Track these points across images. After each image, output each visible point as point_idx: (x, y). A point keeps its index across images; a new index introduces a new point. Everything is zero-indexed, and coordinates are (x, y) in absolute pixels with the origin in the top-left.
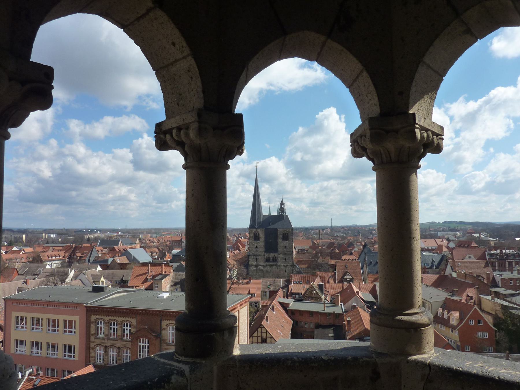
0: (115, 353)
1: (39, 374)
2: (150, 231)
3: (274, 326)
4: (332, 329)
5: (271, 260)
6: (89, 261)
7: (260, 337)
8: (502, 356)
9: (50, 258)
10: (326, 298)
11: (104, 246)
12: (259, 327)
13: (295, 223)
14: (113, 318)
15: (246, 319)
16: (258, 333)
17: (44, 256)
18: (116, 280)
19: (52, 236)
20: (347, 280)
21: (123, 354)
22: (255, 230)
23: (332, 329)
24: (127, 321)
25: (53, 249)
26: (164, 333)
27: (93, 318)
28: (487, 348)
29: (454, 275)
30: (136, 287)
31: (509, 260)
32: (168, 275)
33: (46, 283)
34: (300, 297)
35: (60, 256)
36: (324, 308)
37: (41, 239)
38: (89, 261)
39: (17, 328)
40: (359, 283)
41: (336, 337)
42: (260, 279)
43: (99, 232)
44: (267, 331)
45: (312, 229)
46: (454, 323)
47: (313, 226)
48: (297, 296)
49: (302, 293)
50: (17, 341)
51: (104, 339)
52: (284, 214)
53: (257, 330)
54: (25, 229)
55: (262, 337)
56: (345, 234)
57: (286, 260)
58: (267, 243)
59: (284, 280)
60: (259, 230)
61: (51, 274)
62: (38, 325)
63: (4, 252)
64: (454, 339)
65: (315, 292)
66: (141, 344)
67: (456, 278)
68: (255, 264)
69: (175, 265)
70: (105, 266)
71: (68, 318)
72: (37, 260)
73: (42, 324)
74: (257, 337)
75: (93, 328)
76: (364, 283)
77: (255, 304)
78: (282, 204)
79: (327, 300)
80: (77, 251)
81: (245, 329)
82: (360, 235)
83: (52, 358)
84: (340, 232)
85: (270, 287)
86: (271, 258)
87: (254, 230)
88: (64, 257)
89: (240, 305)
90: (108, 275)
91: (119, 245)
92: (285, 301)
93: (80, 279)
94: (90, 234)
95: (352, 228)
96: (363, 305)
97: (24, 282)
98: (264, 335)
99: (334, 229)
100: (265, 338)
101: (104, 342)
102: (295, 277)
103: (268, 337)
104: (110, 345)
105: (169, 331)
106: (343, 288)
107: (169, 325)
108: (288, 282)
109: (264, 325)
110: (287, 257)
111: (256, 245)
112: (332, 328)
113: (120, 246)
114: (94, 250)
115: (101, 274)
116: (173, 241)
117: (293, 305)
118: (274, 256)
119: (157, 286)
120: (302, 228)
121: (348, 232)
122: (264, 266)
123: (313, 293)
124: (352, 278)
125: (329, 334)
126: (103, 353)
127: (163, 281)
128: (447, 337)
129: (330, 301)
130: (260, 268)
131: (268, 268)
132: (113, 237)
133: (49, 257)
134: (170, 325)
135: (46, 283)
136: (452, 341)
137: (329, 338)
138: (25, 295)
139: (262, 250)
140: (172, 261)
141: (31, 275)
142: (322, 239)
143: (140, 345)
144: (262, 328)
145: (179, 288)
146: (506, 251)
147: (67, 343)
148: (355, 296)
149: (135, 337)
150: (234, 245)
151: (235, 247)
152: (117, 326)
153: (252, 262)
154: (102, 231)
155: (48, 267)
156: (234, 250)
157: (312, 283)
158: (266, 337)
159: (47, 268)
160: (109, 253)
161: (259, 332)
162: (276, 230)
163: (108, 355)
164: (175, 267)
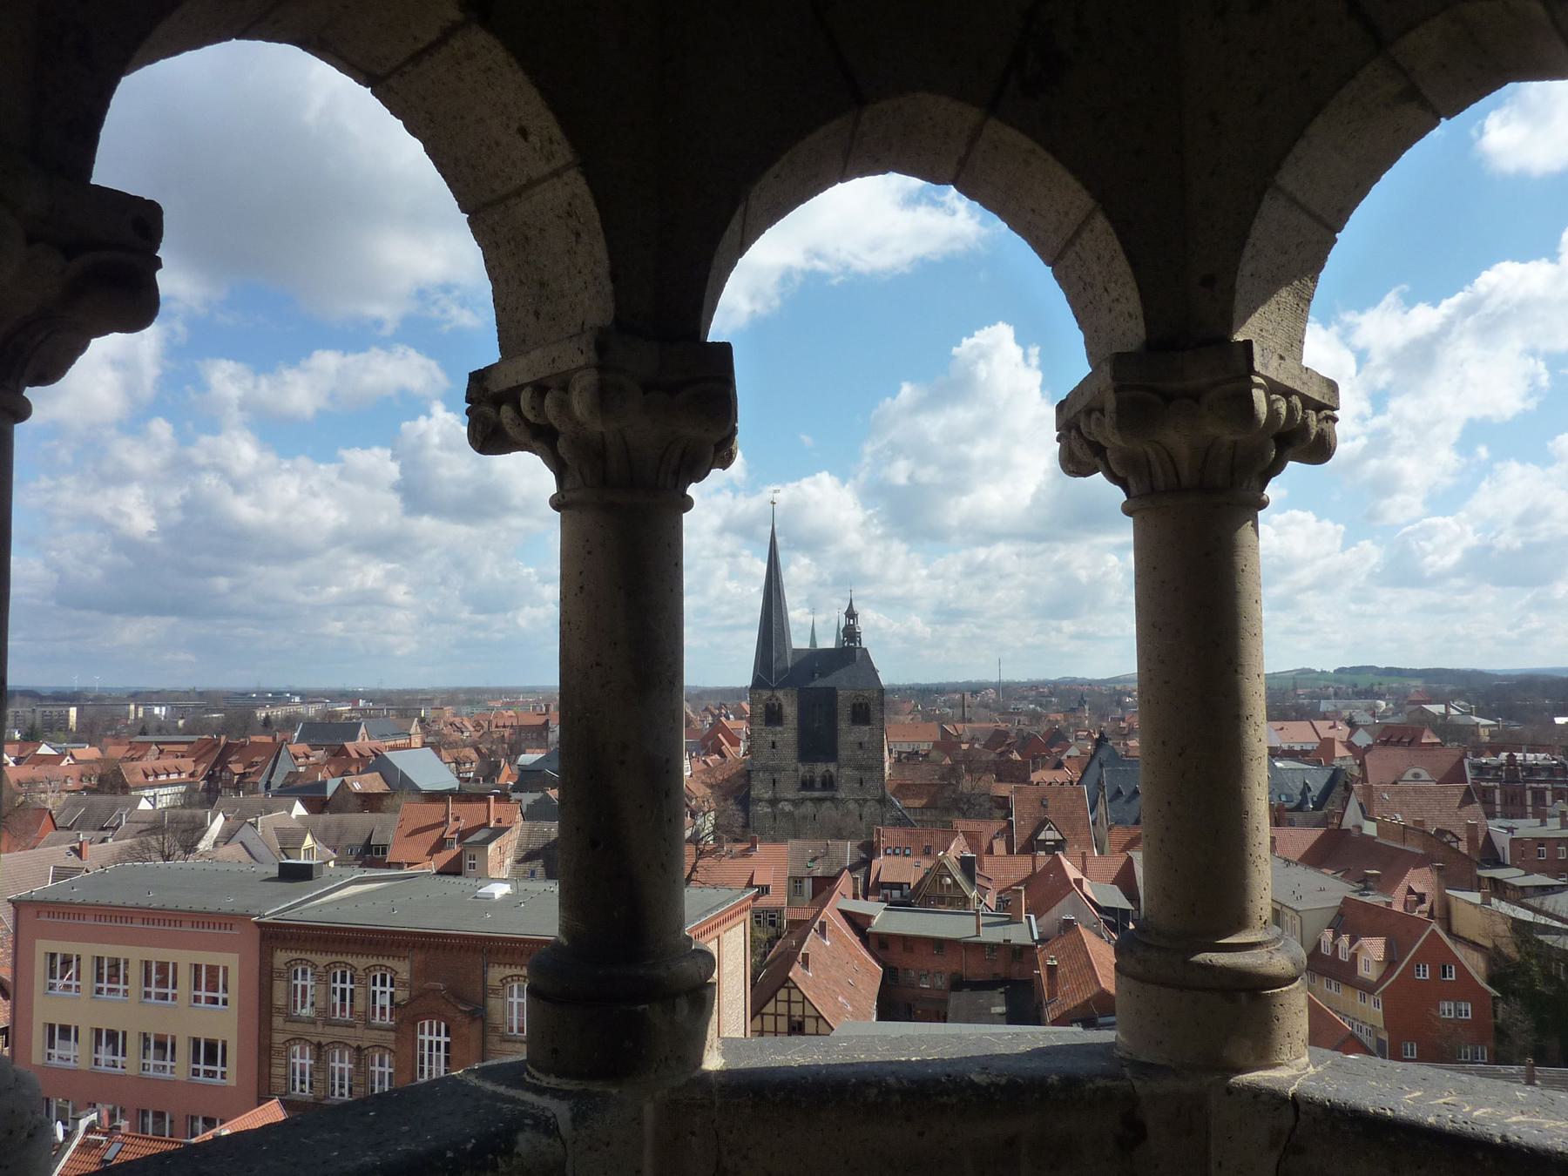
0: (347, 1066)
1: (119, 1128)
2: (452, 697)
3: (825, 982)
4: (1001, 993)
5: (818, 784)
6: (268, 786)
7: (783, 1015)
8: (1513, 1074)
9: (151, 779)
10: (984, 898)
11: (313, 741)
12: (782, 986)
13: (890, 673)
14: (340, 958)
15: (740, 963)
16: (778, 1003)
17: (132, 772)
18: (349, 846)
19: (157, 710)
20: (1047, 843)
21: (372, 1068)
22: (770, 693)
23: (1001, 993)
24: (384, 968)
25: (161, 752)
26: (493, 1003)
27: (281, 958)
29: (1370, 829)
30: (409, 865)
31: (1534, 785)
32: (507, 829)
33: (139, 853)
34: (906, 897)
35: (180, 773)
36: (978, 927)
37: (124, 721)
38: (268, 786)
39: (50, 988)
40: (1084, 853)
41: (1013, 1017)
42: (783, 840)
43: (297, 699)
44: (805, 997)
45: (940, 690)
46: (1369, 973)
47: (944, 682)
48: (896, 894)
49: (909, 884)
50: (52, 1027)
51: (313, 1022)
52: (855, 644)
53: (775, 994)
54: (76, 690)
55: (790, 1016)
56: (1041, 706)
57: (861, 783)
58: (804, 731)
59: (858, 843)
60: (780, 694)
61: (155, 825)
62: (115, 979)
63: (13, 758)
64: (1369, 1023)
65: (949, 881)
66: (426, 1038)
67: (1374, 838)
68: (768, 795)
69: (529, 798)
70: (317, 802)
71: (206, 958)
72: (112, 783)
73: (126, 977)
74: (776, 1015)
75: (280, 989)
76: (1096, 855)
77: (770, 916)
78: (851, 614)
79: (985, 904)
80: (233, 758)
81: (738, 992)
82: (1087, 707)
83: (157, 1080)
84: (1025, 698)
85: (814, 865)
86: (818, 779)
87: (766, 694)
88: (192, 775)
89: (725, 921)
90: (327, 828)
91: (360, 740)
92: (861, 906)
93: (241, 842)
94: (272, 706)
95: (1062, 687)
96: (1096, 920)
97: (73, 849)
98: (797, 1010)
99: (1007, 690)
100: (800, 1019)
101: (312, 1030)
102: (889, 836)
103: (809, 1017)
104: (333, 1040)
105: (510, 999)
106: (1034, 868)
107: (509, 979)
108: (869, 851)
109: (795, 979)
110: (867, 776)
111: (771, 738)
112: (1002, 990)
113: (362, 742)
114: (283, 753)
115: (306, 827)
116: (521, 727)
117: (883, 918)
118: (828, 771)
119: (472, 862)
120: (911, 688)
121: (1049, 699)
122: (797, 803)
123: (943, 882)
124: (1061, 838)
125: (992, 1008)
126: (311, 1065)
127: (491, 847)
128: (1348, 1016)
129: (994, 908)
130: (783, 809)
131: (808, 808)
132: (341, 713)
133: (147, 776)
134: (513, 980)
135: (139, 853)
136: (1364, 1027)
137: (992, 1020)
138: (75, 890)
139: (789, 754)
140: (518, 788)
141: (94, 830)
142: (970, 721)
143: (422, 1042)
144: (789, 989)
145: (540, 870)
146: (1525, 756)
147: (203, 1035)
148: (1071, 894)
149: (407, 1016)
150: (704, 740)
151: (710, 743)
152: (352, 983)
153: (760, 790)
154: (307, 697)
155: (144, 805)
156: (707, 754)
157: (942, 853)
158: (804, 1016)
159: (140, 807)
160: (328, 763)
161: (780, 1001)
162: (831, 693)
163: (325, 1071)
164: (528, 805)
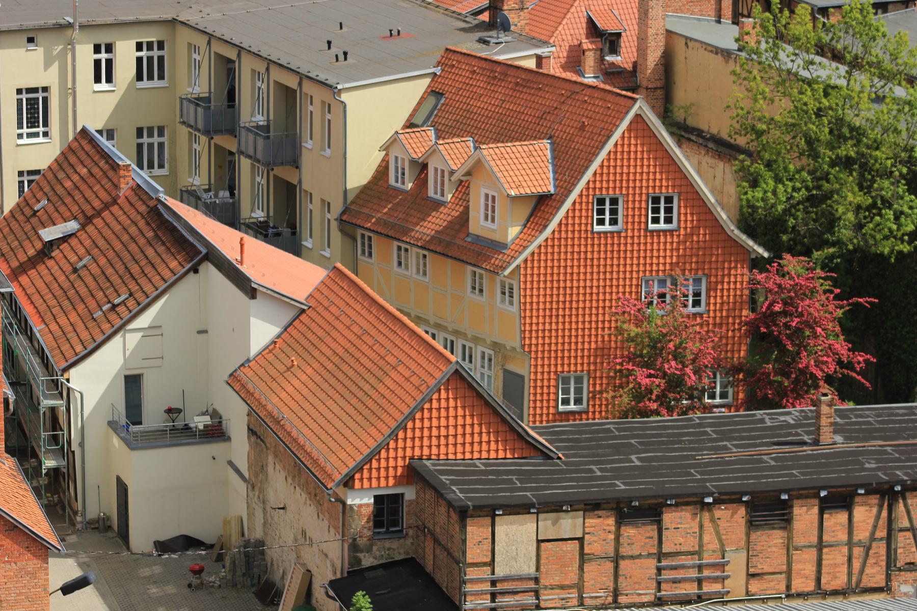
8: (789, 426)
28: (870, 419)
46: (494, 226)
64: (432, 320)
128: (463, 335)
136: (478, 351)
